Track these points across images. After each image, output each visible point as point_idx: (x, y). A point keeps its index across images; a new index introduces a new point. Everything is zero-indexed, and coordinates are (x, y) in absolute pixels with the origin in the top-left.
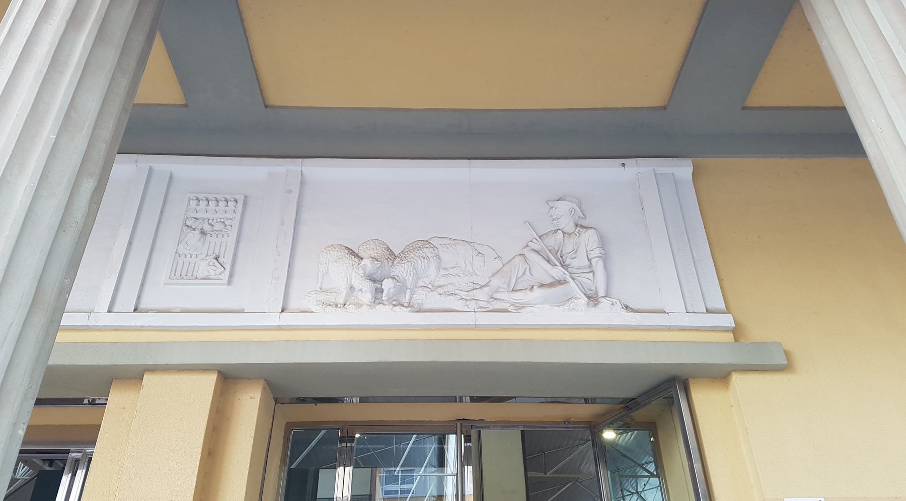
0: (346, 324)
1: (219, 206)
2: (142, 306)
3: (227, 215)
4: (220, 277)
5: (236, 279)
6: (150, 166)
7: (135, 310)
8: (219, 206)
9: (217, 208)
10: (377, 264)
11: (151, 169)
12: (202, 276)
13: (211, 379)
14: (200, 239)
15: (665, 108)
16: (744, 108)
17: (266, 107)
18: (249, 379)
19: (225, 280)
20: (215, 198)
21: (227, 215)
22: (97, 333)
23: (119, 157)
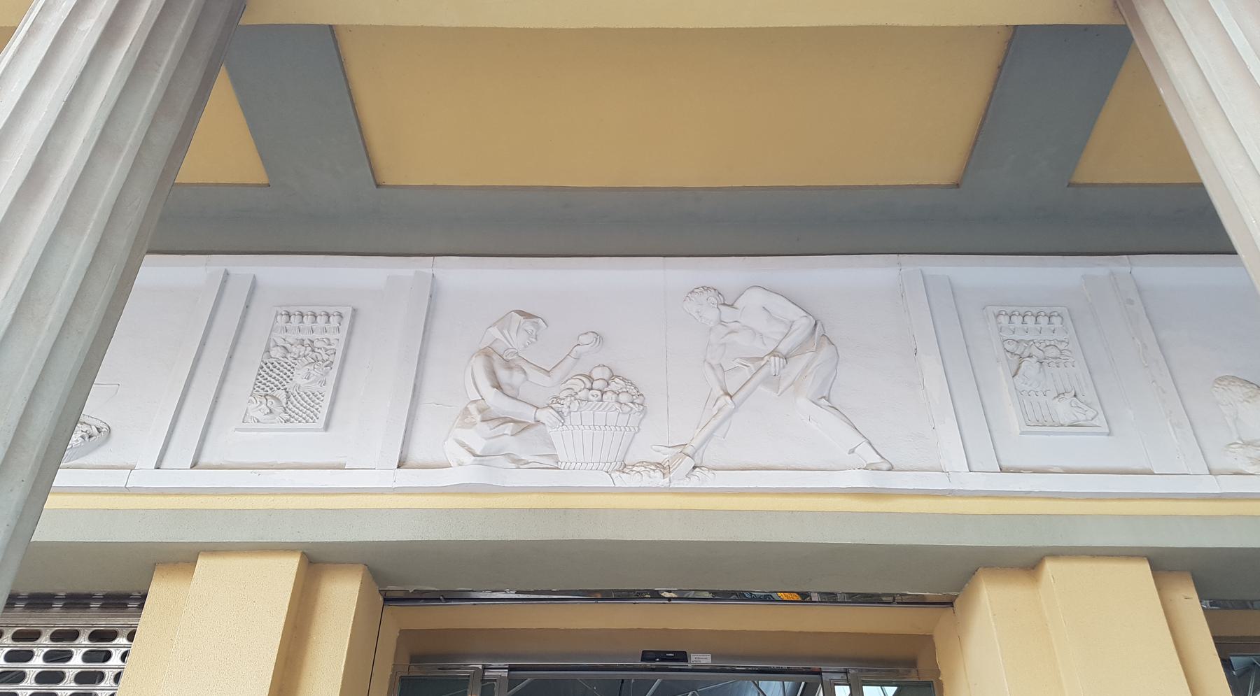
0: (638, 486)
1: (303, 323)
2: (410, 462)
3: (1055, 336)
4: (1093, 422)
5: (485, 423)
6: (226, 270)
7: (194, 466)
8: (303, 323)
9: (288, 326)
10: (591, 404)
11: (227, 274)
12: (1068, 421)
13: (291, 564)
14: (1040, 371)
15: (958, 186)
16: (1069, 185)
17: (378, 186)
18: (1170, 571)
19: (321, 423)
20: (312, 312)
21: (1055, 336)
22: (960, 501)
23: (148, 258)
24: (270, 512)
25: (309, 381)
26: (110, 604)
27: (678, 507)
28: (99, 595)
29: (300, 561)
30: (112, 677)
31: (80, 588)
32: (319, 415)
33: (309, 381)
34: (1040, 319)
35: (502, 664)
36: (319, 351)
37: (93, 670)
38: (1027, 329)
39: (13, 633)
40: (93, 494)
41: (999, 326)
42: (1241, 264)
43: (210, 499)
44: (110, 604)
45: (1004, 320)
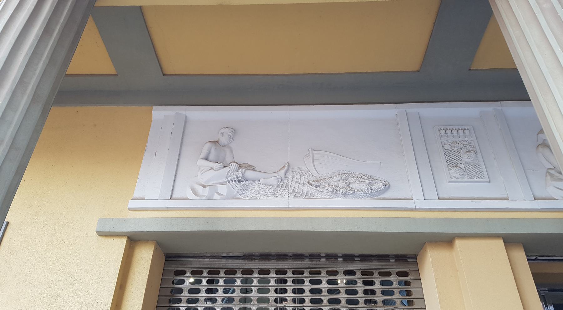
13: (123, 242)
17: (164, 75)
24: (487, 219)
25: (471, 160)
26: (382, 259)
27: (272, 216)
28: (291, 254)
29: (127, 240)
30: (204, 291)
31: (248, 251)
32: (485, 176)
33: (471, 160)
34: (453, 131)
35: (546, 289)
36: (466, 146)
37: (388, 289)
38: (460, 136)
39: (224, 271)
40: (398, 211)
41: (440, 135)
42: (532, 106)
43: (454, 213)
44: (382, 259)
45: (442, 132)
